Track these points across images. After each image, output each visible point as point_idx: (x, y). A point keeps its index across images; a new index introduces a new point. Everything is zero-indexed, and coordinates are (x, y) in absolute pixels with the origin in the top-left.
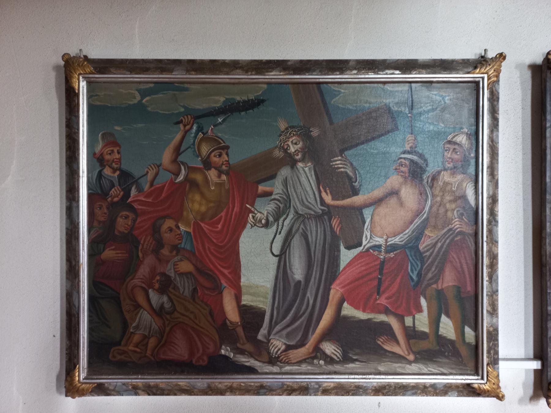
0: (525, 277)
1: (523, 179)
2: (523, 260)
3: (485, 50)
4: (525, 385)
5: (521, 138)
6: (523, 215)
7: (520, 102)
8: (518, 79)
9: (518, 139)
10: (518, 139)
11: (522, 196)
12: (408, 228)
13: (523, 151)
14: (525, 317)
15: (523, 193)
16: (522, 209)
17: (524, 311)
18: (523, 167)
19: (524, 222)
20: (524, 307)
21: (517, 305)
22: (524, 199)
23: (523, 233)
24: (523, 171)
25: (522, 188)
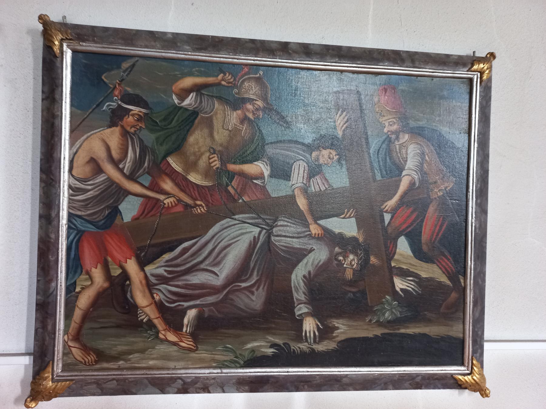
0: (30, 263)
1: (33, 155)
2: (29, 245)
3: (474, 52)
4: (23, 382)
5: (32, 110)
6: (30, 195)
7: (31, 72)
8: (30, 46)
9: (28, 111)
10: (28, 111)
11: (31, 174)
12: (475, 212)
13: (33, 125)
14: (28, 308)
15: (32, 171)
16: (30, 188)
17: (27, 301)
18: (34, 142)
19: (31, 203)
20: (27, 296)
21: (19, 294)
22: (33, 178)
23: (30, 214)
24: (33, 147)
25: (30, 166)
